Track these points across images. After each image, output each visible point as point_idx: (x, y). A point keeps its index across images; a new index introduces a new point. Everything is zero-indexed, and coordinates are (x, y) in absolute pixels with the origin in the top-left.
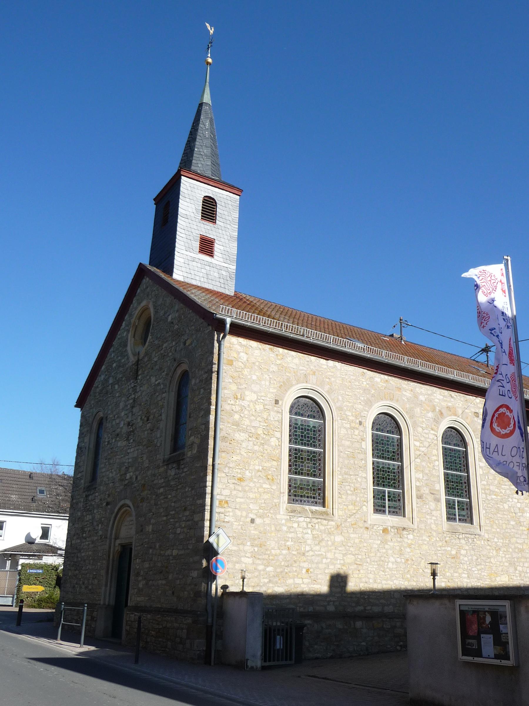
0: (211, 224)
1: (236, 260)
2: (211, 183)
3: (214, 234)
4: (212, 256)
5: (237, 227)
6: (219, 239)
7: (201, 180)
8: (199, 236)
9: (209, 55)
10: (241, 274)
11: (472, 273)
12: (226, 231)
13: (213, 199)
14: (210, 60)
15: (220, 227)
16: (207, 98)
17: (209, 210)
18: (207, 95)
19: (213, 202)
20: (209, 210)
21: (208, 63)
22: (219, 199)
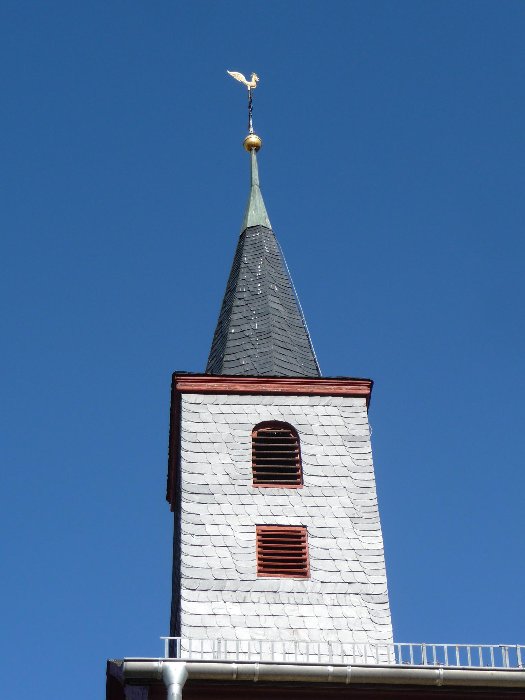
0: (287, 490)
1: (383, 565)
2: (271, 388)
3: (301, 511)
4: (305, 574)
5: (372, 476)
6: (318, 522)
7: (239, 387)
8: (254, 529)
9: (252, 129)
10: (411, 606)
11: (249, 89)
12: (339, 494)
13: (286, 425)
14: (254, 139)
15: (316, 491)
16: (257, 214)
17: (276, 457)
18: (256, 209)
19: (287, 434)
20: (276, 457)
21: (251, 147)
22: (302, 420)
